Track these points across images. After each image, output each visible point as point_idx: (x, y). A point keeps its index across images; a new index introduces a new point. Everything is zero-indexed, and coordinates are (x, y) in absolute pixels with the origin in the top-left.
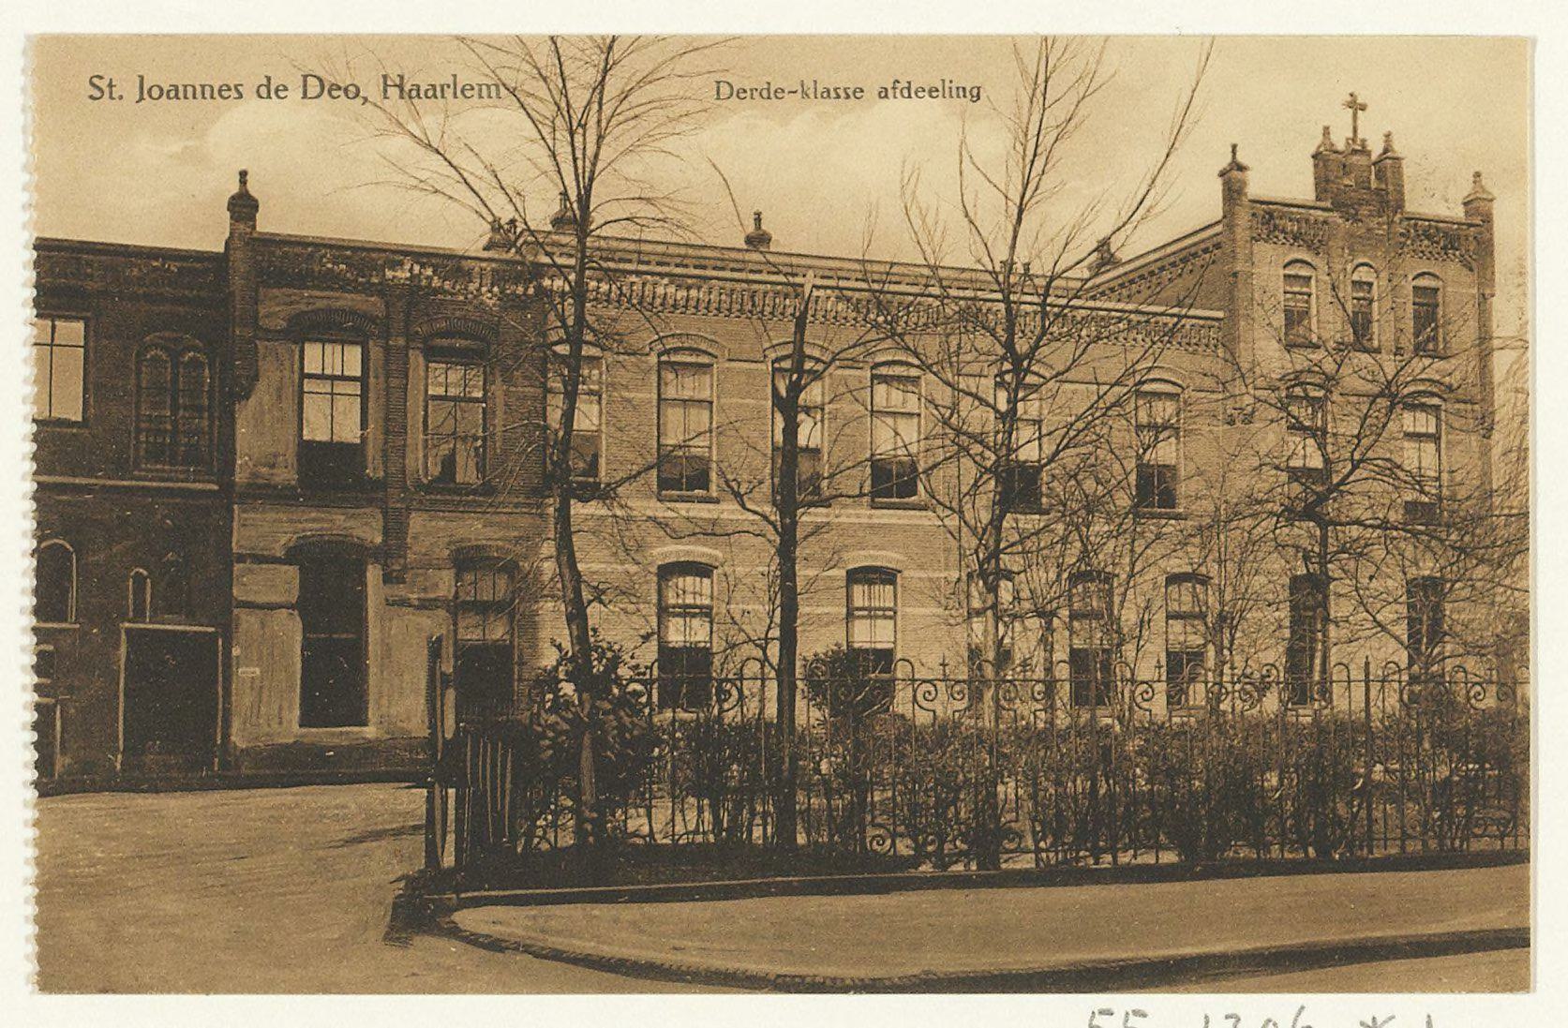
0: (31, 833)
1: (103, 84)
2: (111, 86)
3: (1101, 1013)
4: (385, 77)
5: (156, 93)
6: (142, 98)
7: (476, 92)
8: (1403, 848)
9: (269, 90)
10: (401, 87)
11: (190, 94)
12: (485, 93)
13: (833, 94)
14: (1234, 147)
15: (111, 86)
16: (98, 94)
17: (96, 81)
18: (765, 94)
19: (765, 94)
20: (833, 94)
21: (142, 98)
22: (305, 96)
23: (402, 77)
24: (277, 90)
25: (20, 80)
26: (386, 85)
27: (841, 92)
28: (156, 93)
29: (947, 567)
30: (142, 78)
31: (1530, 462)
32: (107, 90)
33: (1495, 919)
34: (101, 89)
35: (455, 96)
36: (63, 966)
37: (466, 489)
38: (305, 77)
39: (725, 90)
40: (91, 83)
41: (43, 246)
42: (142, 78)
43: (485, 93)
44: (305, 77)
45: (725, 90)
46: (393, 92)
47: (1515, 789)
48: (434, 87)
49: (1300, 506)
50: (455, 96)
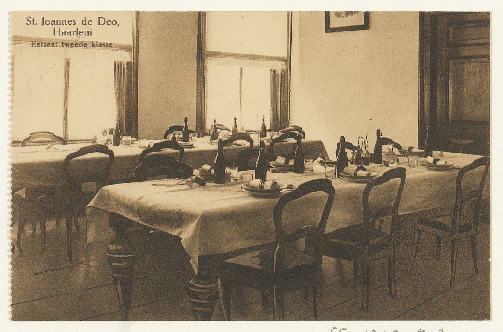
0: (10, 179)
1: (31, 19)
2: (33, 20)
3: (343, 329)
5: (48, 22)
6: (43, 24)
7: (84, 34)
11: (59, 23)
17: (28, 18)
21: (43, 24)
22: (99, 24)
24: (68, 22)
26: (55, 31)
30: (43, 18)
32: (32, 22)
35: (60, 35)
38: (99, 18)
39: (102, 21)
41: (205, 13)
42: (43, 18)
44: (99, 18)
45: (102, 21)
47: (486, 219)
50: (60, 35)
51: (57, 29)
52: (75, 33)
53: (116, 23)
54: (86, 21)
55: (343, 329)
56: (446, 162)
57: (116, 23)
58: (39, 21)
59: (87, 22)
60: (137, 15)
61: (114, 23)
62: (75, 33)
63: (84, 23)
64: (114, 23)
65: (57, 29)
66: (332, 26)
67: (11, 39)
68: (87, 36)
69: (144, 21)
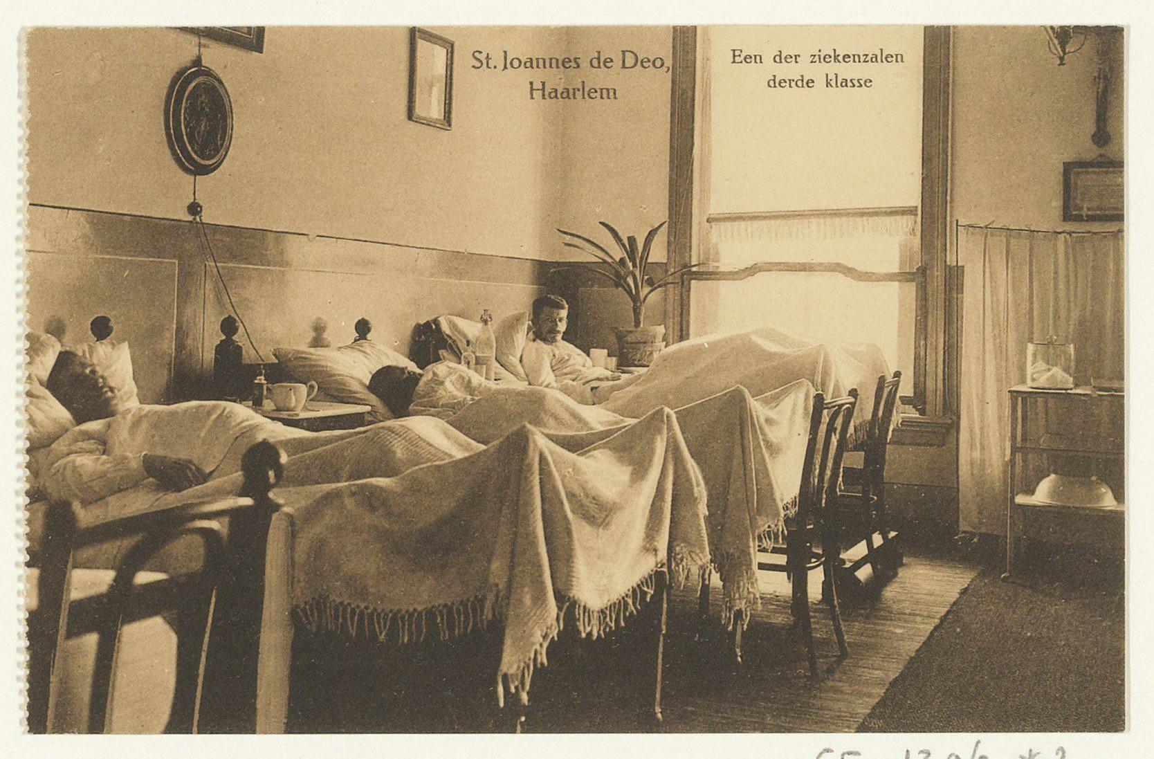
1: (482, 57)
4: (531, 83)
5: (516, 63)
6: (505, 67)
12: (605, 96)
14: (857, 754)
16: (478, 64)
18: (800, 83)
19: (800, 83)
20: (849, 84)
22: (624, 67)
23: (543, 84)
24: (605, 61)
25: (18, 103)
26: (532, 89)
27: (855, 82)
28: (516, 63)
29: (1089, 209)
31: (1125, 233)
32: (485, 62)
36: (1105, 713)
39: (630, 61)
40: (1129, 27)
43: (605, 96)
45: (630, 61)
46: (537, 94)
51: (537, 85)
53: (662, 65)
54: (599, 58)
55: (849, 753)
56: (194, 209)
57: (662, 65)
58: (498, 60)
59: (602, 62)
60: (939, 44)
61: (658, 63)
63: (595, 64)
64: (658, 63)
66: (421, 45)
67: (25, 68)
68: (606, 101)
69: (965, 67)
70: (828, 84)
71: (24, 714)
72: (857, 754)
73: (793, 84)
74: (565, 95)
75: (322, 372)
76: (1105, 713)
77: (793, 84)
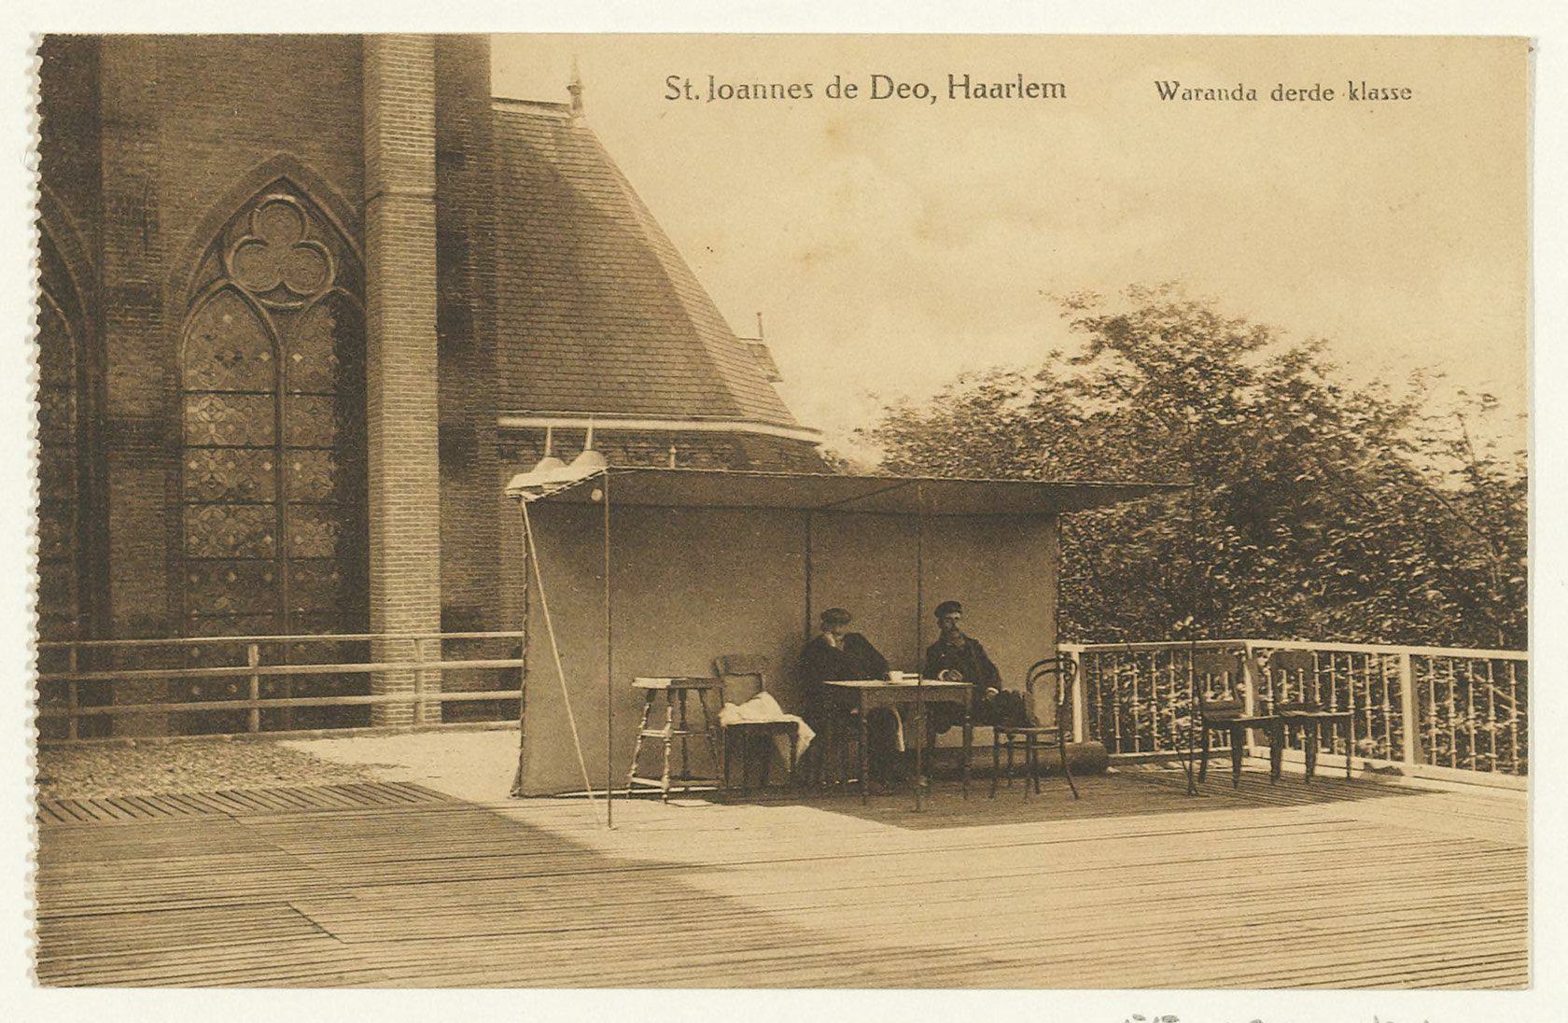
1: (680, 84)
2: (687, 86)
5: (726, 92)
8: (968, 736)
9: (842, 90)
10: (967, 86)
11: (760, 93)
12: (1049, 92)
13: (1381, 95)
14: (1058, 90)
15: (687, 86)
16: (674, 94)
17: (672, 81)
18: (1314, 95)
19: (1314, 95)
20: (1381, 95)
28: (726, 92)
33: (1494, 940)
34: (677, 89)
37: (1293, 779)
38: (874, 77)
39: (883, 88)
43: (1049, 92)
44: (874, 77)
45: (883, 88)
46: (959, 92)
48: (1000, 87)
49: (1389, 428)
51: (959, 80)
52: (1014, 91)
58: (700, 88)
61: (921, 91)
62: (1014, 91)
64: (921, 91)
65: (959, 80)
70: (1353, 96)
71: (31, 963)
72: (1058, 90)
73: (1305, 96)
74: (743, 94)
75: (609, 221)
76: (1514, 55)
77: (1305, 96)
